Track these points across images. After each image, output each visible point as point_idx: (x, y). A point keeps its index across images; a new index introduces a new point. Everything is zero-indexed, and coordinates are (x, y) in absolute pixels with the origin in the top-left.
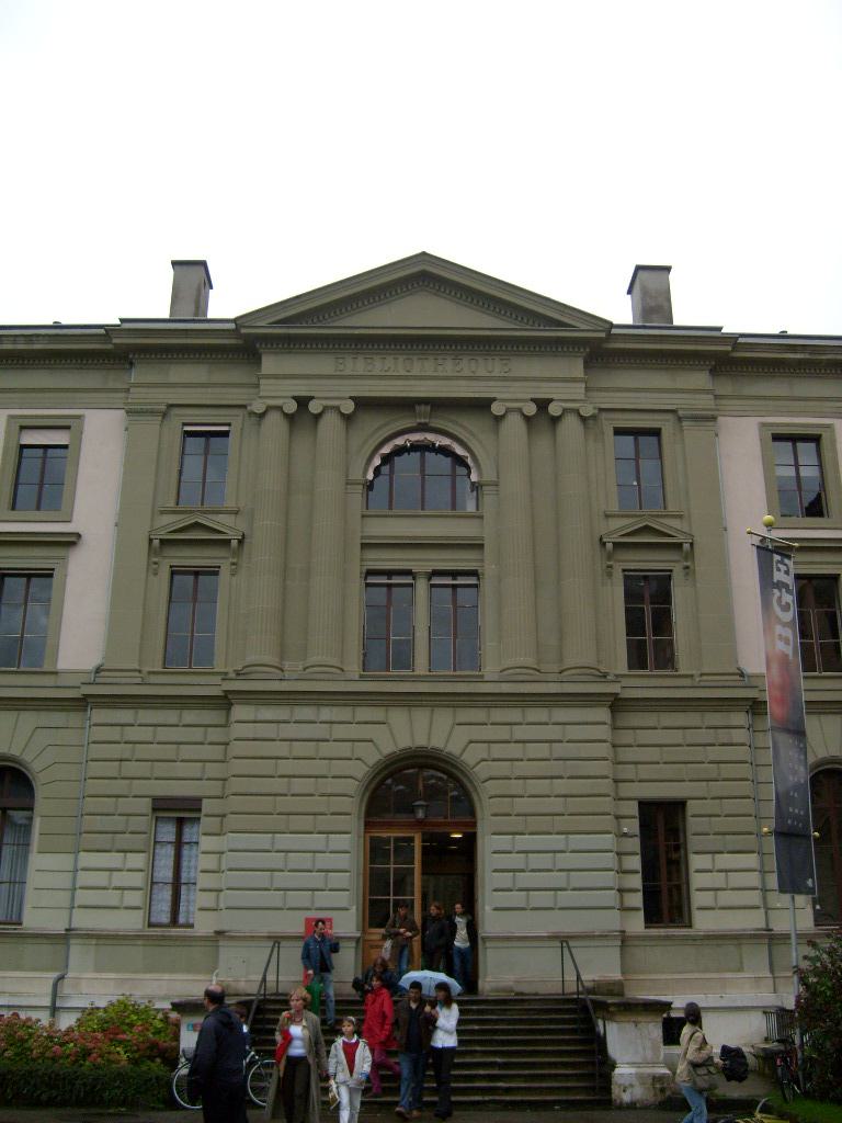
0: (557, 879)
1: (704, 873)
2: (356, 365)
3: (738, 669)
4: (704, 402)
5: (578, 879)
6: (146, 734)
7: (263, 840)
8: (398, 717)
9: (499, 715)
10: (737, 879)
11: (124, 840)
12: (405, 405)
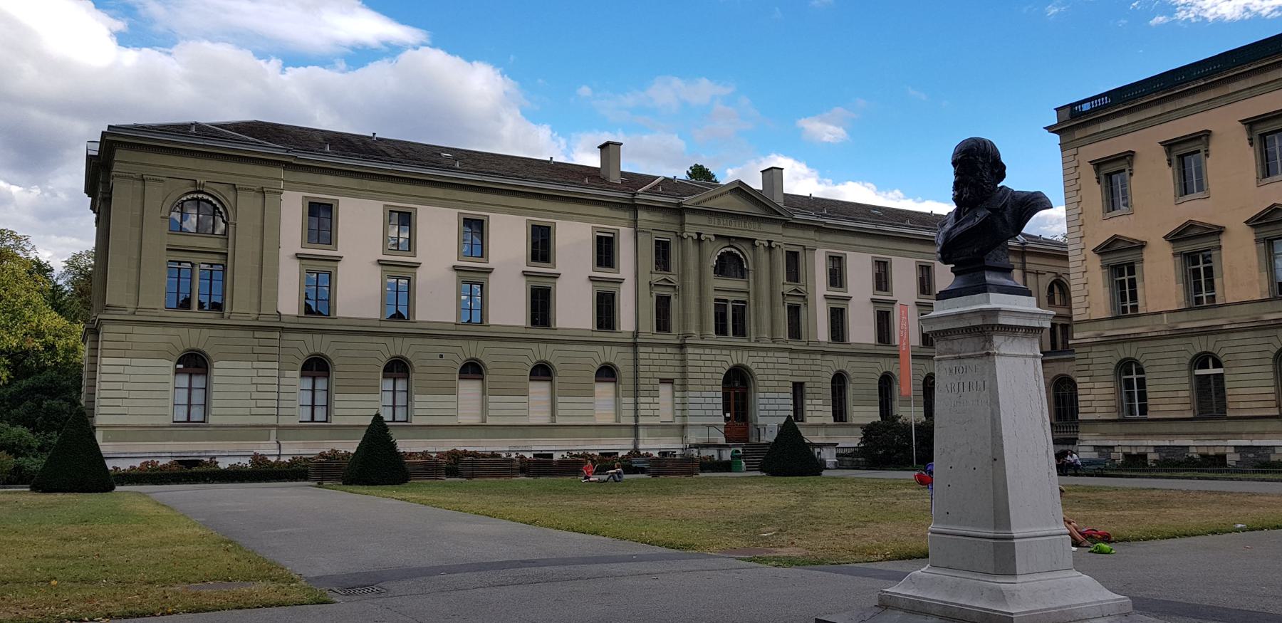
0: (776, 407)
2: (715, 221)
3: (278, 312)
6: (656, 356)
12: (728, 238)
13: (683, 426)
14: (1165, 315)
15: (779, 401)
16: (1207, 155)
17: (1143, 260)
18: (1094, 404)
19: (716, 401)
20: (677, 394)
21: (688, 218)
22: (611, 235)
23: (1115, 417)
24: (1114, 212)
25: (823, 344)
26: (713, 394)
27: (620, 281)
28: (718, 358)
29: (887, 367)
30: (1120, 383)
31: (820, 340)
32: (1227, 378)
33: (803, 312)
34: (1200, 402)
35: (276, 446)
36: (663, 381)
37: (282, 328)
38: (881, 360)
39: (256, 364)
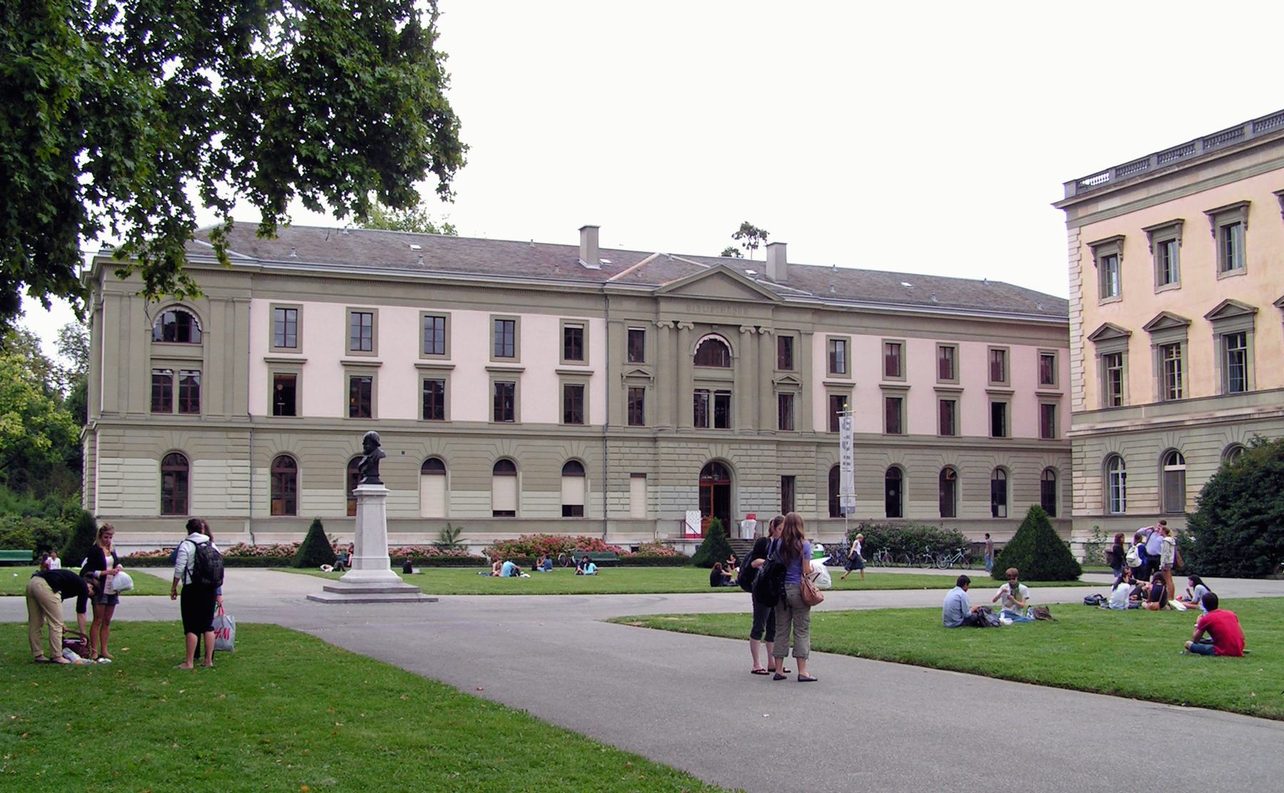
0: (760, 502)
1: (800, 499)
2: (694, 308)
4: (808, 327)
5: (766, 502)
6: (627, 450)
7: (671, 488)
8: (712, 446)
9: (743, 446)
10: (810, 502)
11: (690, 482)
12: (711, 325)
13: (605, 521)
14: (1143, 408)
15: (762, 496)
16: (1246, 228)
17: (1128, 350)
18: (1086, 499)
19: (691, 495)
20: (650, 489)
21: (664, 306)
22: (580, 327)
23: (1100, 513)
24: (1231, 271)
25: (822, 436)
26: (688, 488)
27: (589, 374)
28: (695, 451)
29: (1117, 448)
30: (1108, 477)
31: (816, 430)
32: (1187, 475)
33: (796, 402)
34: (1167, 498)
35: (250, 537)
36: (634, 475)
37: (254, 429)
38: (889, 451)
39: (231, 462)
